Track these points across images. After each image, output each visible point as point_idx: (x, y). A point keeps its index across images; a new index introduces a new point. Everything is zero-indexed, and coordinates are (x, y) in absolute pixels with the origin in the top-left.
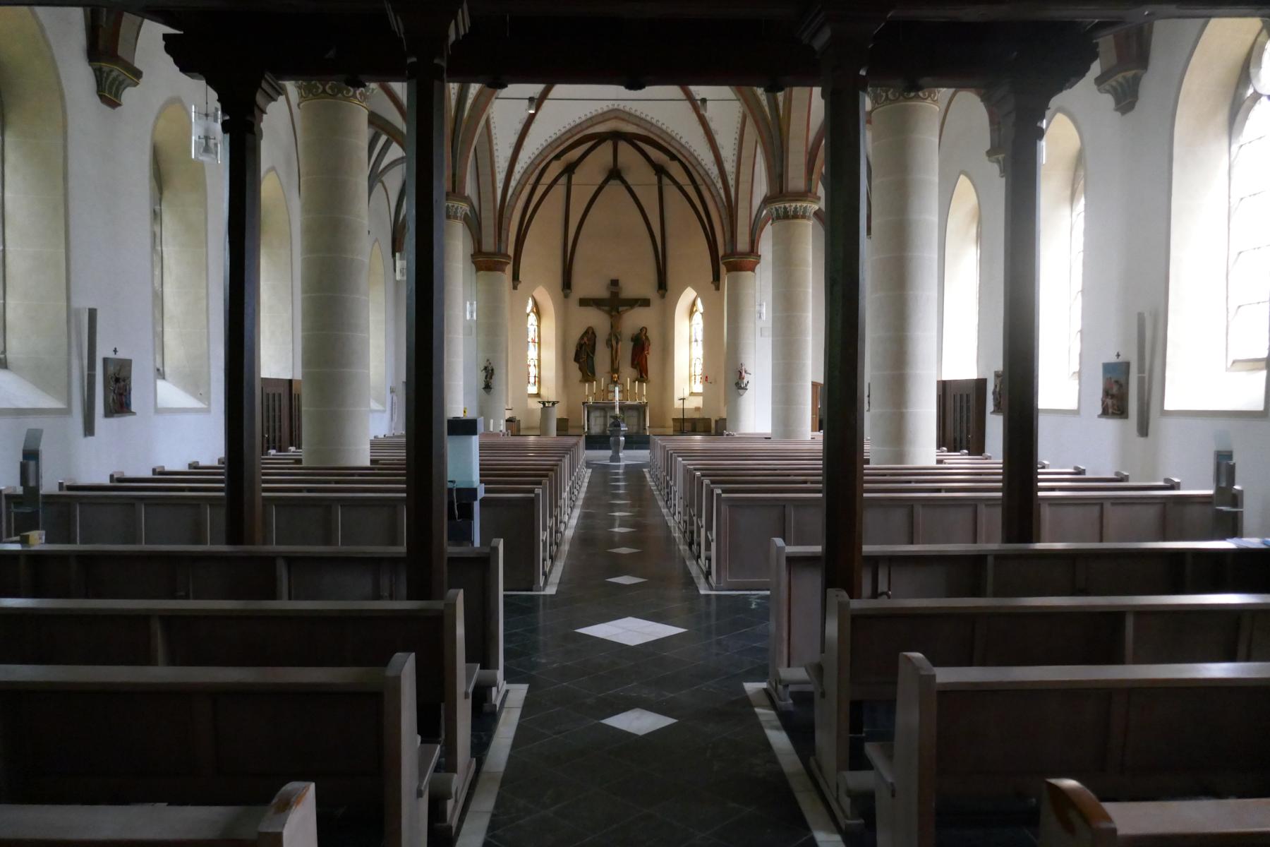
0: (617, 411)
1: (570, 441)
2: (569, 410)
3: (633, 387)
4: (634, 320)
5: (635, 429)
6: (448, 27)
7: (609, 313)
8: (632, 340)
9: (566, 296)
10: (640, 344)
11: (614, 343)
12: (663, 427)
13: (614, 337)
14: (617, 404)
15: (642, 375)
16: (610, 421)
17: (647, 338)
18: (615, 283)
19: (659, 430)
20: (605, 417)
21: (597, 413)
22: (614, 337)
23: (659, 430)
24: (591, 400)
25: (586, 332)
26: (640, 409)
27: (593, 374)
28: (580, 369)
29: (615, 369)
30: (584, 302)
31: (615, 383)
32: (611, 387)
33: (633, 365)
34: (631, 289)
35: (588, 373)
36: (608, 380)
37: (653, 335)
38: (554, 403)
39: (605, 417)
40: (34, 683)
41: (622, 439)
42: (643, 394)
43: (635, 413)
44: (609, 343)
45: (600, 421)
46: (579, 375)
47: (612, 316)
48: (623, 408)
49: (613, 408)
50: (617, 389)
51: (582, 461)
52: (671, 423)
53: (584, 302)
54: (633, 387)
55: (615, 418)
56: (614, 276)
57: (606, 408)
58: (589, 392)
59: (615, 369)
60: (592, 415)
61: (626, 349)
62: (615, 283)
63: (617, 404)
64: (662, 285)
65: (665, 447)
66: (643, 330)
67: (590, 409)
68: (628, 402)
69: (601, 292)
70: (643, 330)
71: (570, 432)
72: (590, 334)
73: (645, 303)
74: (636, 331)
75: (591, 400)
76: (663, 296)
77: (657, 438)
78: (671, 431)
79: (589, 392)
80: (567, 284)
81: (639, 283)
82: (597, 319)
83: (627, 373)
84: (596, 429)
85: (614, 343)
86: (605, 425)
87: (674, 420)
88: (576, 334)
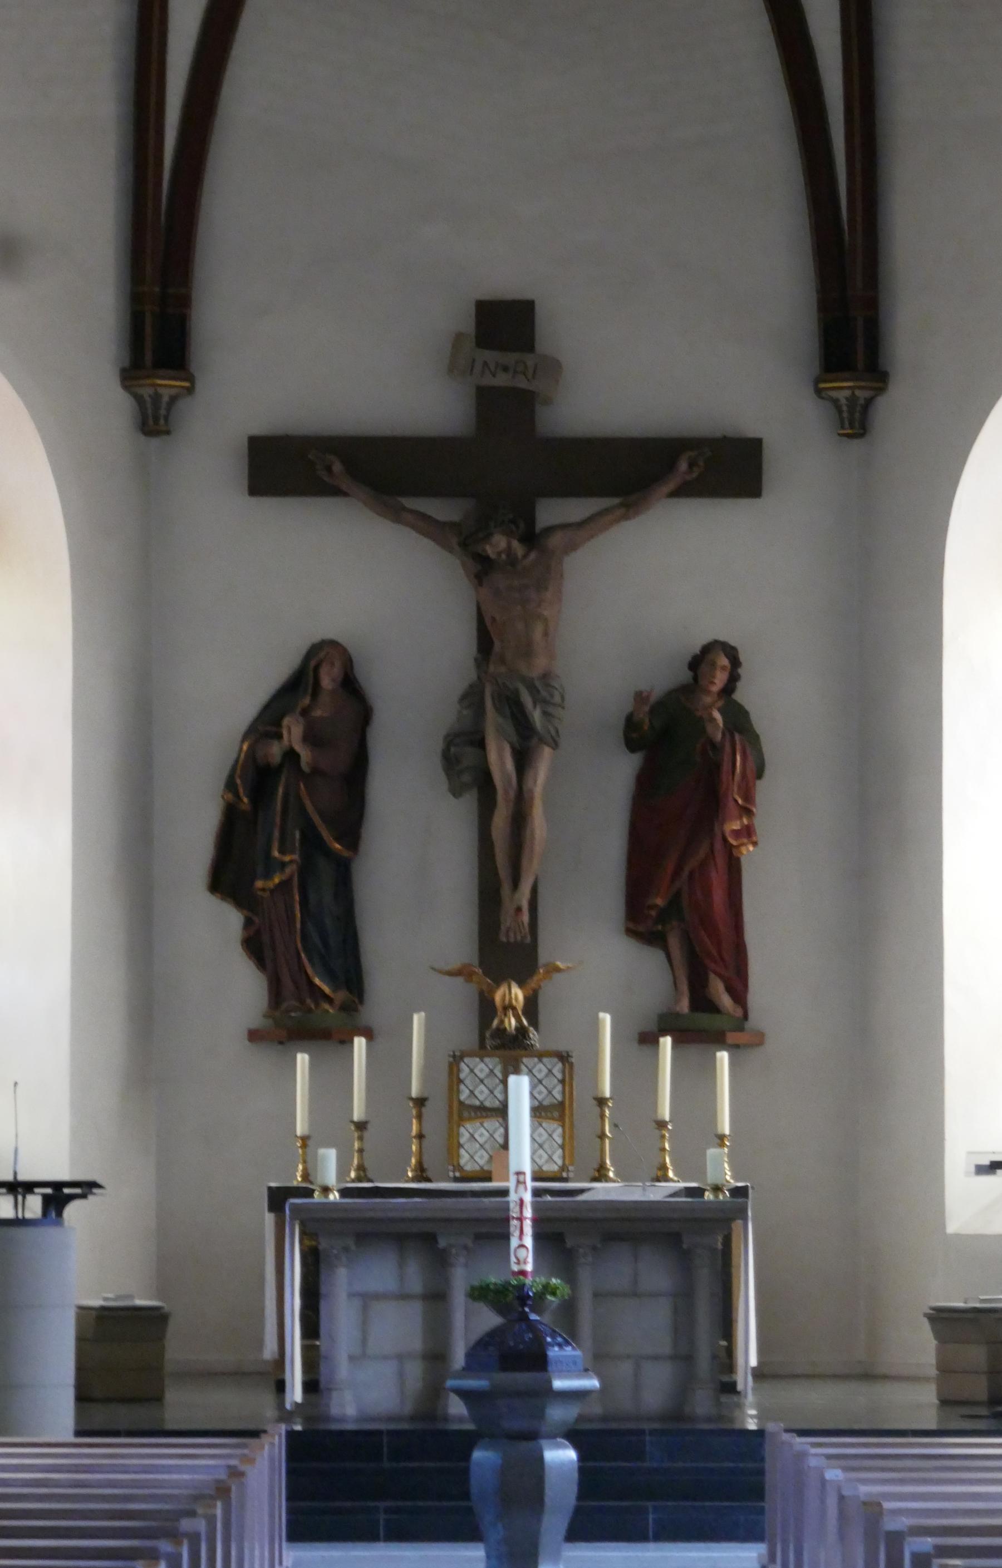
0: (524, 1249)
1: (175, 1468)
2: (171, 1247)
3: (636, 1076)
4: (644, 592)
5: (654, 1390)
6: (725, 722)
7: (467, 542)
8: (633, 736)
9: (154, 422)
10: (690, 757)
11: (500, 760)
12: (868, 1376)
13: (502, 711)
14: (523, 1198)
15: (706, 992)
16: (470, 1323)
17: (739, 721)
18: (505, 325)
19: (818, 1400)
20: (436, 1297)
21: (381, 1272)
22: (502, 711)
23: (818, 1400)
24: (330, 1167)
25: (298, 686)
26: (692, 1239)
27: (352, 979)
28: (255, 946)
29: (504, 949)
30: (284, 466)
31: (511, 1049)
32: (480, 1068)
33: (645, 917)
34: (613, 379)
35: (312, 977)
36: (463, 1031)
37: (784, 700)
38: (58, 1197)
39: (436, 1297)
40: (399, 431)
41: (561, 1456)
42: (706, 1123)
43: (656, 1274)
44: (463, 762)
45: (399, 1328)
46: (241, 989)
47: (482, 569)
48: (563, 1231)
49: (494, 1231)
50: (520, 1089)
51: (323, 1200)
52: (920, 1348)
53: (284, 466)
54: (636, 1076)
55: (510, 1299)
56: (504, 283)
57: (428, 1229)
58: (318, 1117)
59: (504, 949)
60: (341, 1283)
61: (584, 808)
62: (505, 325)
63: (523, 1198)
64: (851, 341)
65: (873, 1510)
66: (714, 662)
67: (328, 1234)
68: (610, 1190)
69: (413, 396)
70: (714, 662)
71: (180, 1404)
72: (322, 703)
73: (729, 468)
74: (663, 676)
75: (330, 1167)
76: (855, 423)
77: (815, 1452)
78: (921, 1403)
79: (318, 1117)
80: (158, 339)
81: (675, 317)
82: (380, 591)
83: (599, 975)
84: (369, 1389)
85: (500, 760)
86: (436, 1357)
87: (943, 1319)
88: (225, 694)
